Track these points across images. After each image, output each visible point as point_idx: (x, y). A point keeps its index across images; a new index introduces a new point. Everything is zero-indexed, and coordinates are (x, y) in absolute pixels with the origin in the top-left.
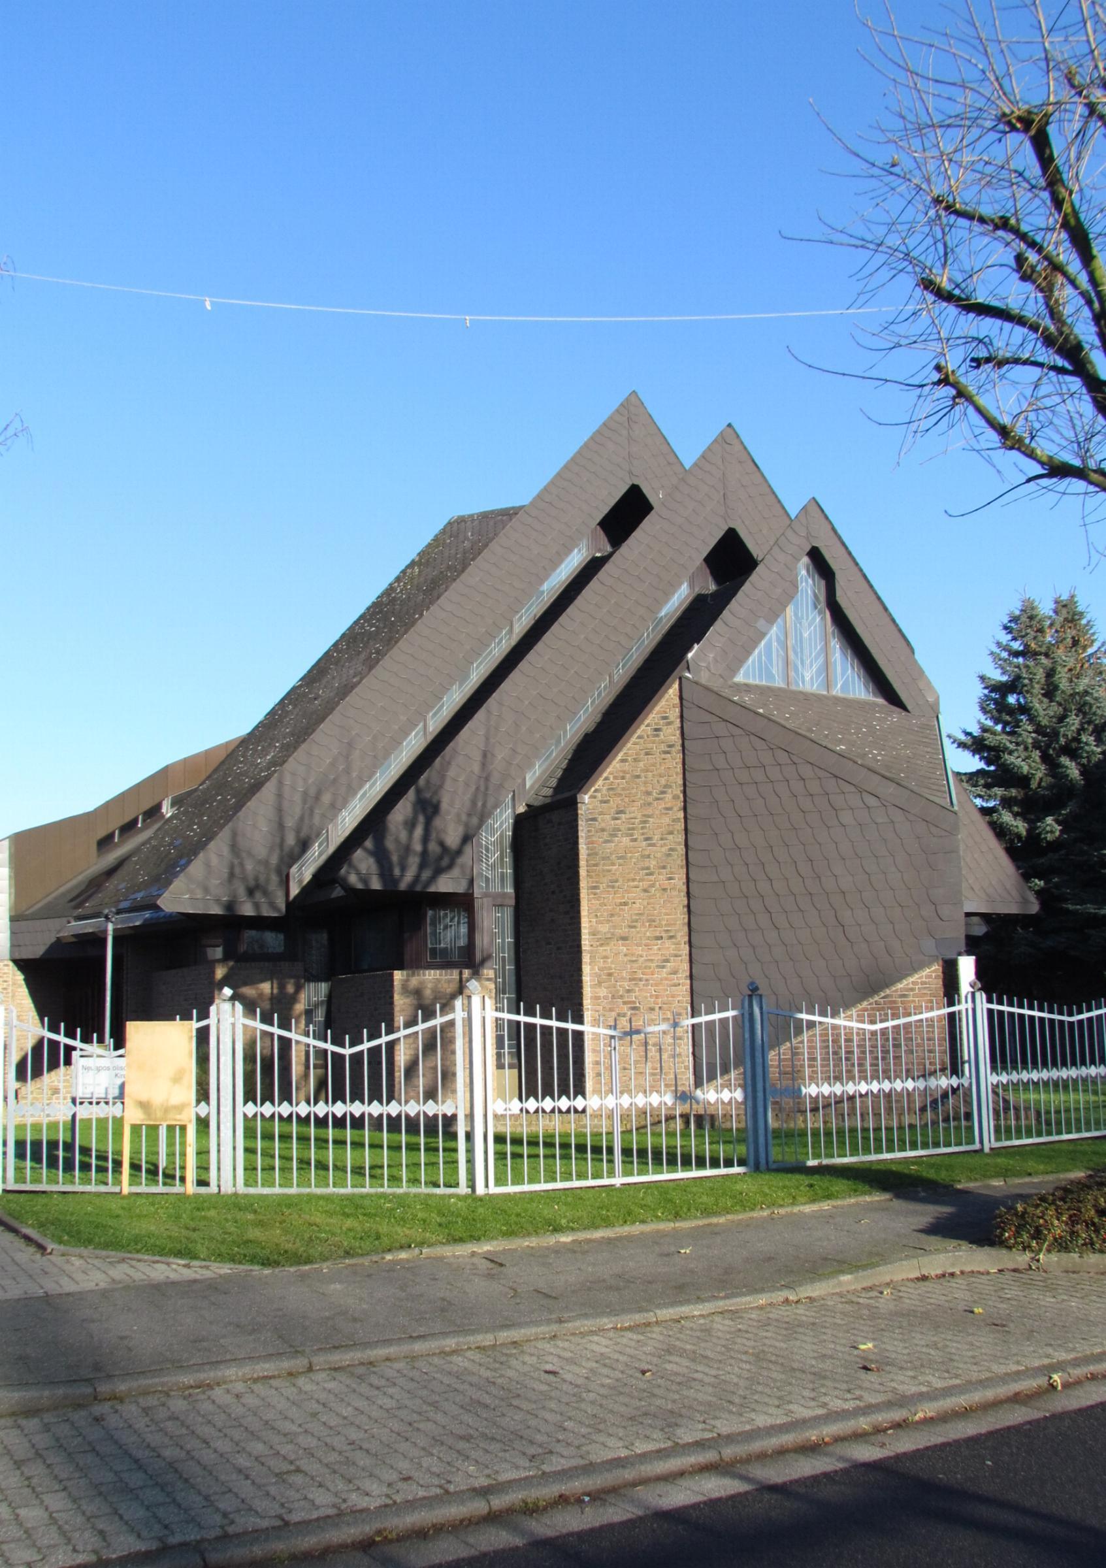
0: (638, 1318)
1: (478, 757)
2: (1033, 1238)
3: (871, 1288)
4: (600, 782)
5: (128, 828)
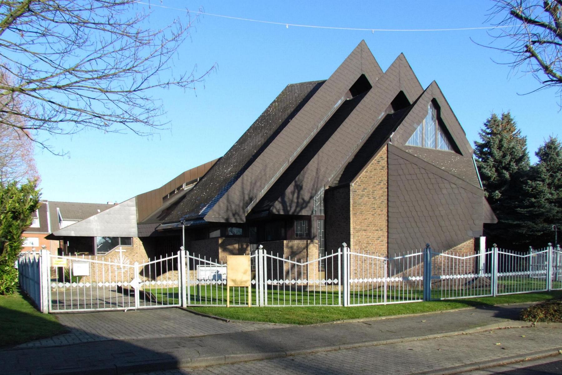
0: (424, 337)
1: (315, 171)
2: (533, 318)
3: (486, 331)
4: (358, 179)
5: (172, 193)
